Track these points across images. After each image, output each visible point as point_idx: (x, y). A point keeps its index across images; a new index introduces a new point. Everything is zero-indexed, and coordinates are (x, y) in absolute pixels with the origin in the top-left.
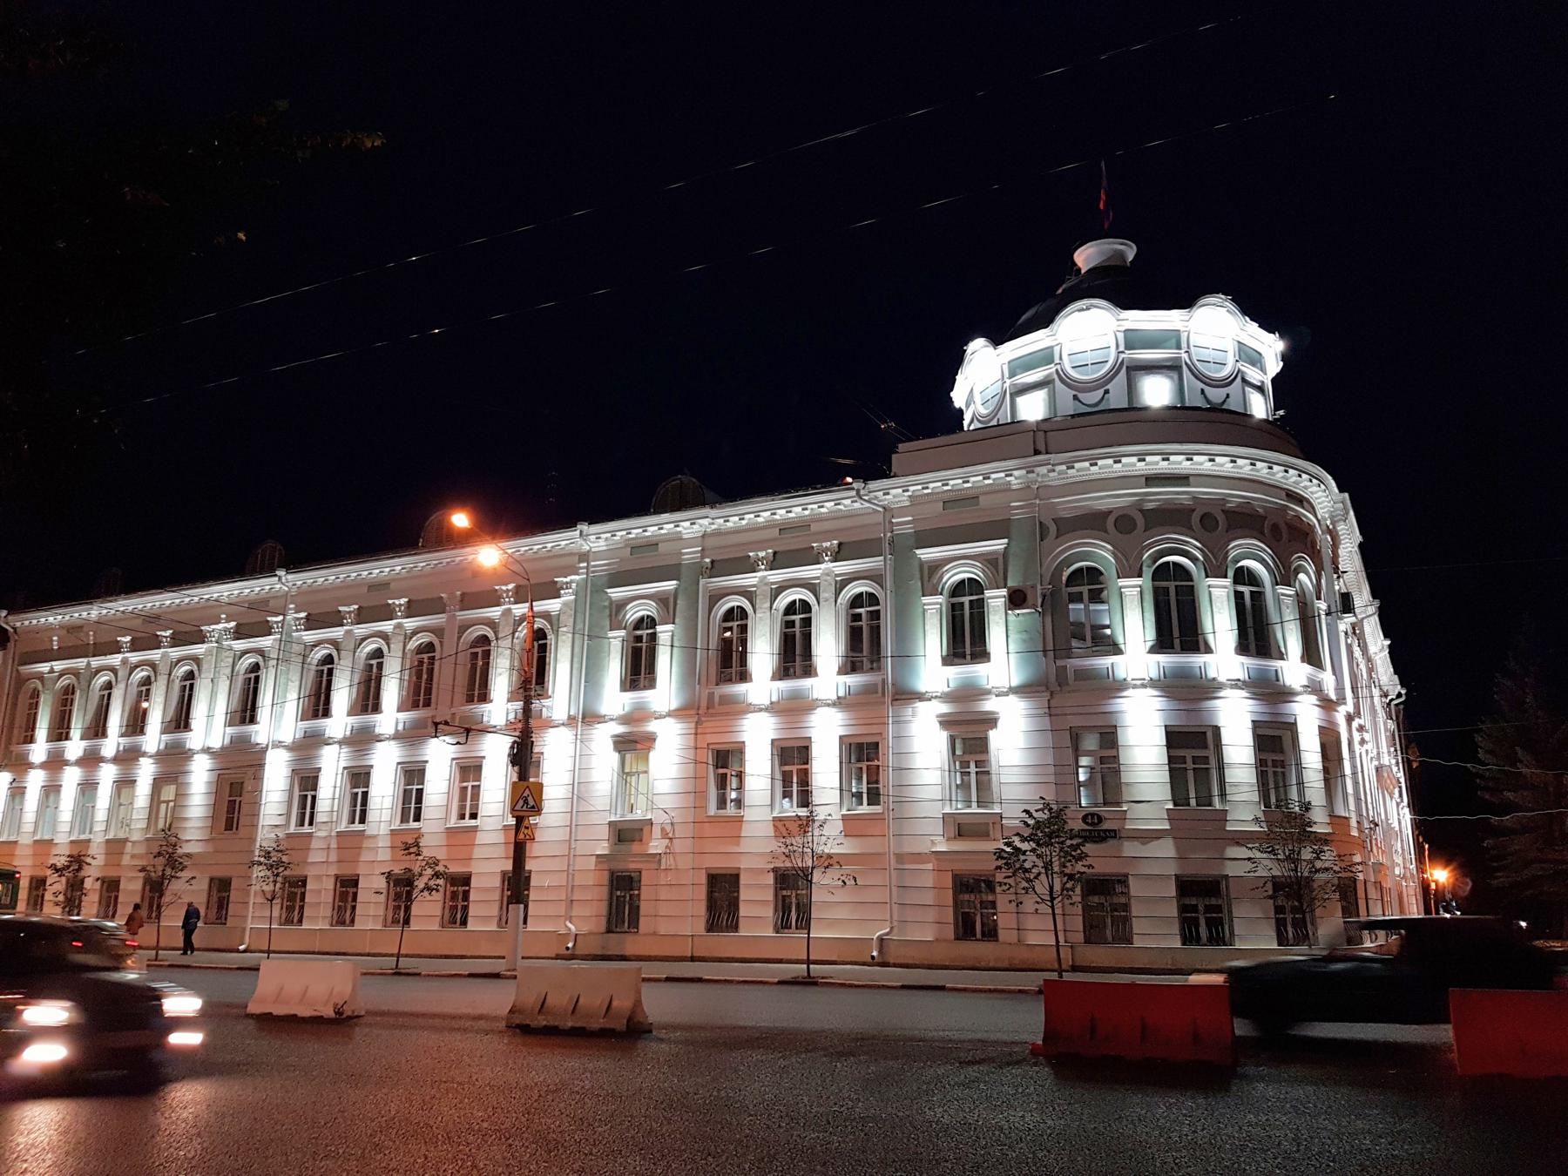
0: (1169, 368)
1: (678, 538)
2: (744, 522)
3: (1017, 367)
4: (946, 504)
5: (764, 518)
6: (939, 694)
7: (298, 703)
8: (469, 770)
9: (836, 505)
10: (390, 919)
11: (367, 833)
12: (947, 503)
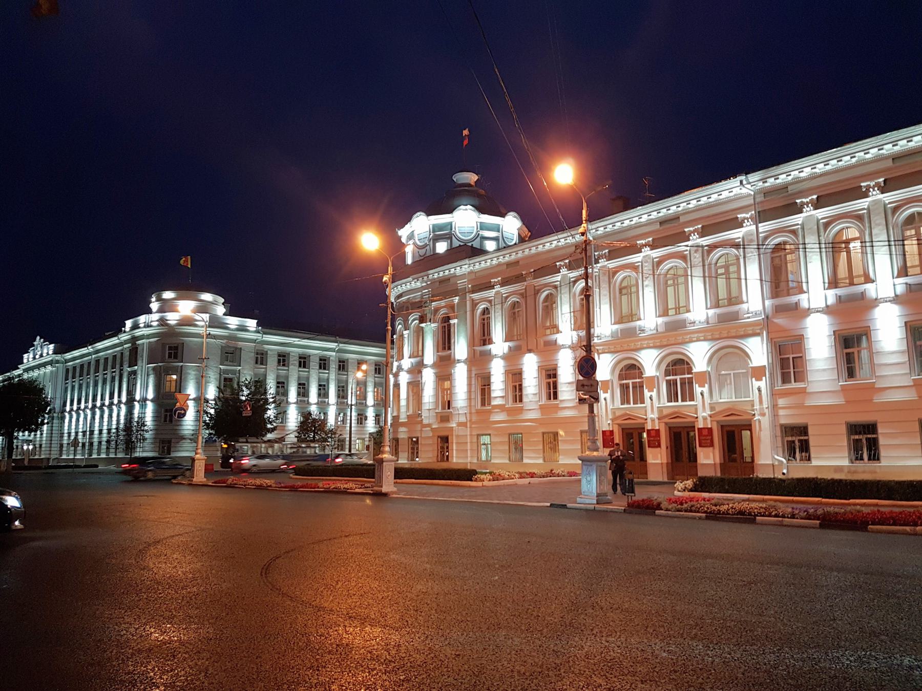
1: (455, 276)
3: (436, 228)
4: (895, 160)
5: (872, 154)
6: (821, 309)
8: (550, 375)
9: (879, 150)
10: (854, 458)
12: (661, 223)
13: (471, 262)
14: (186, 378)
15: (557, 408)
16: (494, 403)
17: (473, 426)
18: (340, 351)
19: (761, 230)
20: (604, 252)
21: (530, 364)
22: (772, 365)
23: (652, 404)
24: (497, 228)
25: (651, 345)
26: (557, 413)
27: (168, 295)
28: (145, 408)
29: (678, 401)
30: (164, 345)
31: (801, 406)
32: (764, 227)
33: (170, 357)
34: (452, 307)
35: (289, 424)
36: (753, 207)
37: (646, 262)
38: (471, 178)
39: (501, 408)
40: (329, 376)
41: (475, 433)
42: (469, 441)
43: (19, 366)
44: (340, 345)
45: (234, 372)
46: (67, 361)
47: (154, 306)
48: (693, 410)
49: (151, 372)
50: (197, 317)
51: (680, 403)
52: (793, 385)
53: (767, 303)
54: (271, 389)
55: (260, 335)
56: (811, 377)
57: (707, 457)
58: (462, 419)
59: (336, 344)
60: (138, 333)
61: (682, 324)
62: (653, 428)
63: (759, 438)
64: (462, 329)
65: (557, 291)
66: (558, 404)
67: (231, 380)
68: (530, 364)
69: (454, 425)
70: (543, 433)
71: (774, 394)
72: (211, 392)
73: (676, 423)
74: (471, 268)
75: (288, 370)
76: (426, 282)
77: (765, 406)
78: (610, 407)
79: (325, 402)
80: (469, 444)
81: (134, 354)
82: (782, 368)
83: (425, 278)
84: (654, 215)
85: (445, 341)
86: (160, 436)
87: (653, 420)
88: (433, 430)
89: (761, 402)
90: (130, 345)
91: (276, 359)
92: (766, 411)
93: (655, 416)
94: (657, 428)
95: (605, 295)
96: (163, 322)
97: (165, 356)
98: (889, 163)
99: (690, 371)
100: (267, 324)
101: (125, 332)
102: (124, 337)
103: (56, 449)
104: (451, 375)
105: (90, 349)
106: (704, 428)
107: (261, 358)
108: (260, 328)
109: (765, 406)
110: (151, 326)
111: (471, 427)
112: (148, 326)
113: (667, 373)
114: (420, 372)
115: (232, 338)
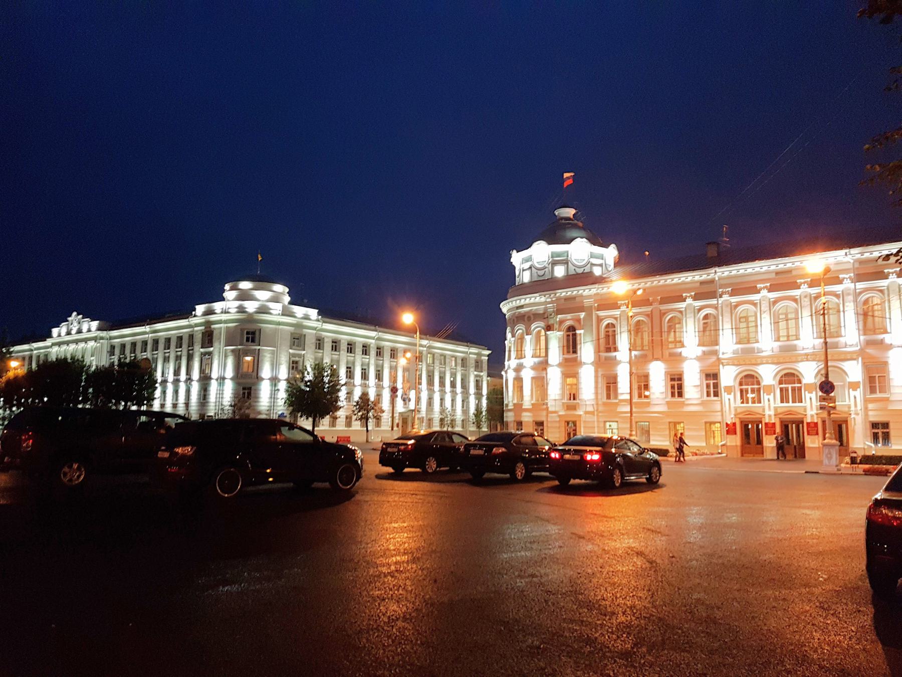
0: (565, 263)
1: (581, 296)
2: (680, 281)
3: (554, 255)
7: (732, 331)
11: (891, 399)
13: (599, 286)
14: (262, 360)
15: (683, 404)
16: (621, 397)
17: (600, 414)
18: (379, 339)
19: (857, 287)
20: (727, 290)
21: (657, 372)
22: (864, 380)
23: (769, 404)
24: (601, 257)
25: (770, 362)
26: (683, 407)
27: (245, 285)
28: (223, 386)
29: (789, 402)
30: (242, 330)
31: (885, 409)
32: (861, 286)
33: (248, 340)
34: (579, 320)
35: (262, 404)
36: (852, 271)
37: (764, 300)
38: (569, 212)
40: (369, 361)
41: (601, 420)
42: (596, 426)
44: (380, 333)
45: (300, 356)
46: (111, 338)
47: (229, 294)
48: (803, 410)
49: (230, 354)
50: (272, 305)
51: (791, 404)
52: (878, 395)
53: (862, 338)
54: (342, 372)
55: (321, 323)
56: (893, 390)
57: (813, 442)
58: (590, 409)
59: (376, 333)
60: (213, 318)
61: (794, 348)
62: (812, 421)
63: (854, 431)
64: (588, 338)
65: (682, 314)
66: (684, 401)
67: (297, 362)
68: (657, 372)
69: (581, 413)
70: (670, 423)
71: (866, 401)
72: (283, 373)
73: (748, 418)
74: (599, 291)
75: (339, 355)
76: (551, 298)
77: (859, 407)
78: (733, 405)
79: (380, 385)
80: (596, 428)
81: (208, 337)
82: (870, 383)
83: (552, 295)
84: (773, 268)
85: (571, 345)
87: (770, 416)
88: (560, 416)
89: (856, 405)
90: (203, 328)
91: (331, 344)
92: (860, 412)
93: (772, 413)
94: (816, 421)
95: (727, 322)
96: (241, 310)
97: (243, 340)
99: (800, 382)
100: (327, 313)
101: (195, 316)
102: (193, 321)
104: (578, 373)
105: (147, 328)
106: (811, 422)
107: (319, 344)
108: (320, 317)
109: (859, 407)
110: (228, 313)
111: (597, 415)
112: (226, 312)
113: (780, 383)
114: (545, 369)
115: (298, 326)
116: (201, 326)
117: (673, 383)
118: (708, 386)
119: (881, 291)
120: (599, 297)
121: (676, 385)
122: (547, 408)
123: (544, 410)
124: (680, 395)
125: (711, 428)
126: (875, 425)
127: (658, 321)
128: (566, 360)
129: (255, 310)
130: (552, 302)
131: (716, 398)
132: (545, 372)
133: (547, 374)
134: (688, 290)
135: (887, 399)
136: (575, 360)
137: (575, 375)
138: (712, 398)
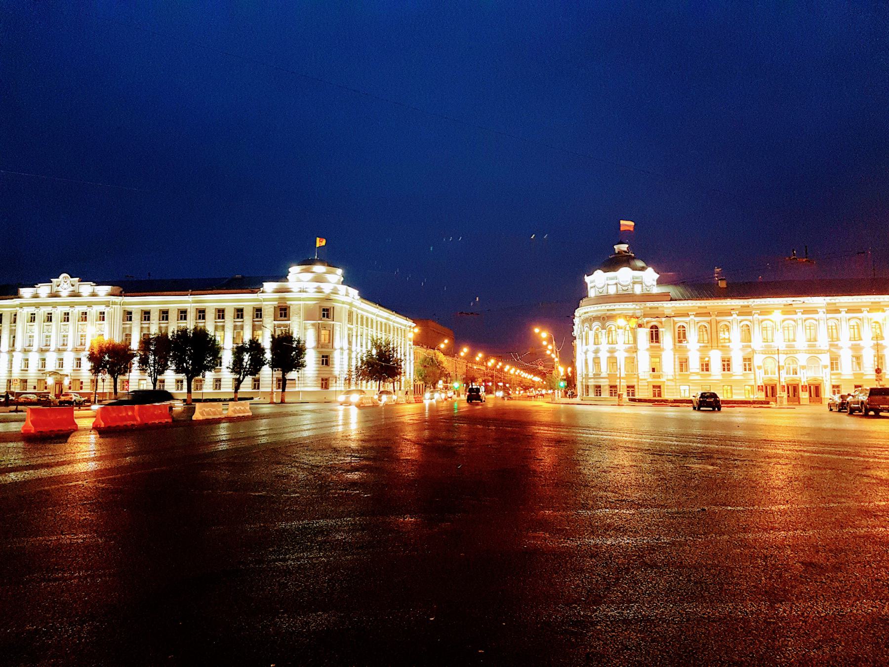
15: (732, 375)
30: (320, 307)
34: (661, 323)
39: (697, 374)
43: (52, 280)
49: (311, 327)
52: (835, 372)
71: (832, 374)
86: (320, 375)
88: (648, 382)
90: (277, 303)
98: (870, 304)
103: (30, 384)
110: (306, 292)
116: (274, 301)
117: (724, 363)
118: (745, 365)
119: (838, 320)
120: (674, 309)
121: (727, 365)
122: (638, 377)
123: (635, 378)
124: (707, 370)
125: (592, 378)
126: (833, 387)
127: (715, 327)
128: (651, 347)
129: (331, 291)
130: (640, 309)
131: (750, 372)
132: (635, 354)
133: (637, 355)
134: (691, 311)
135: (840, 374)
136: (659, 347)
137: (659, 357)
138: (747, 372)
